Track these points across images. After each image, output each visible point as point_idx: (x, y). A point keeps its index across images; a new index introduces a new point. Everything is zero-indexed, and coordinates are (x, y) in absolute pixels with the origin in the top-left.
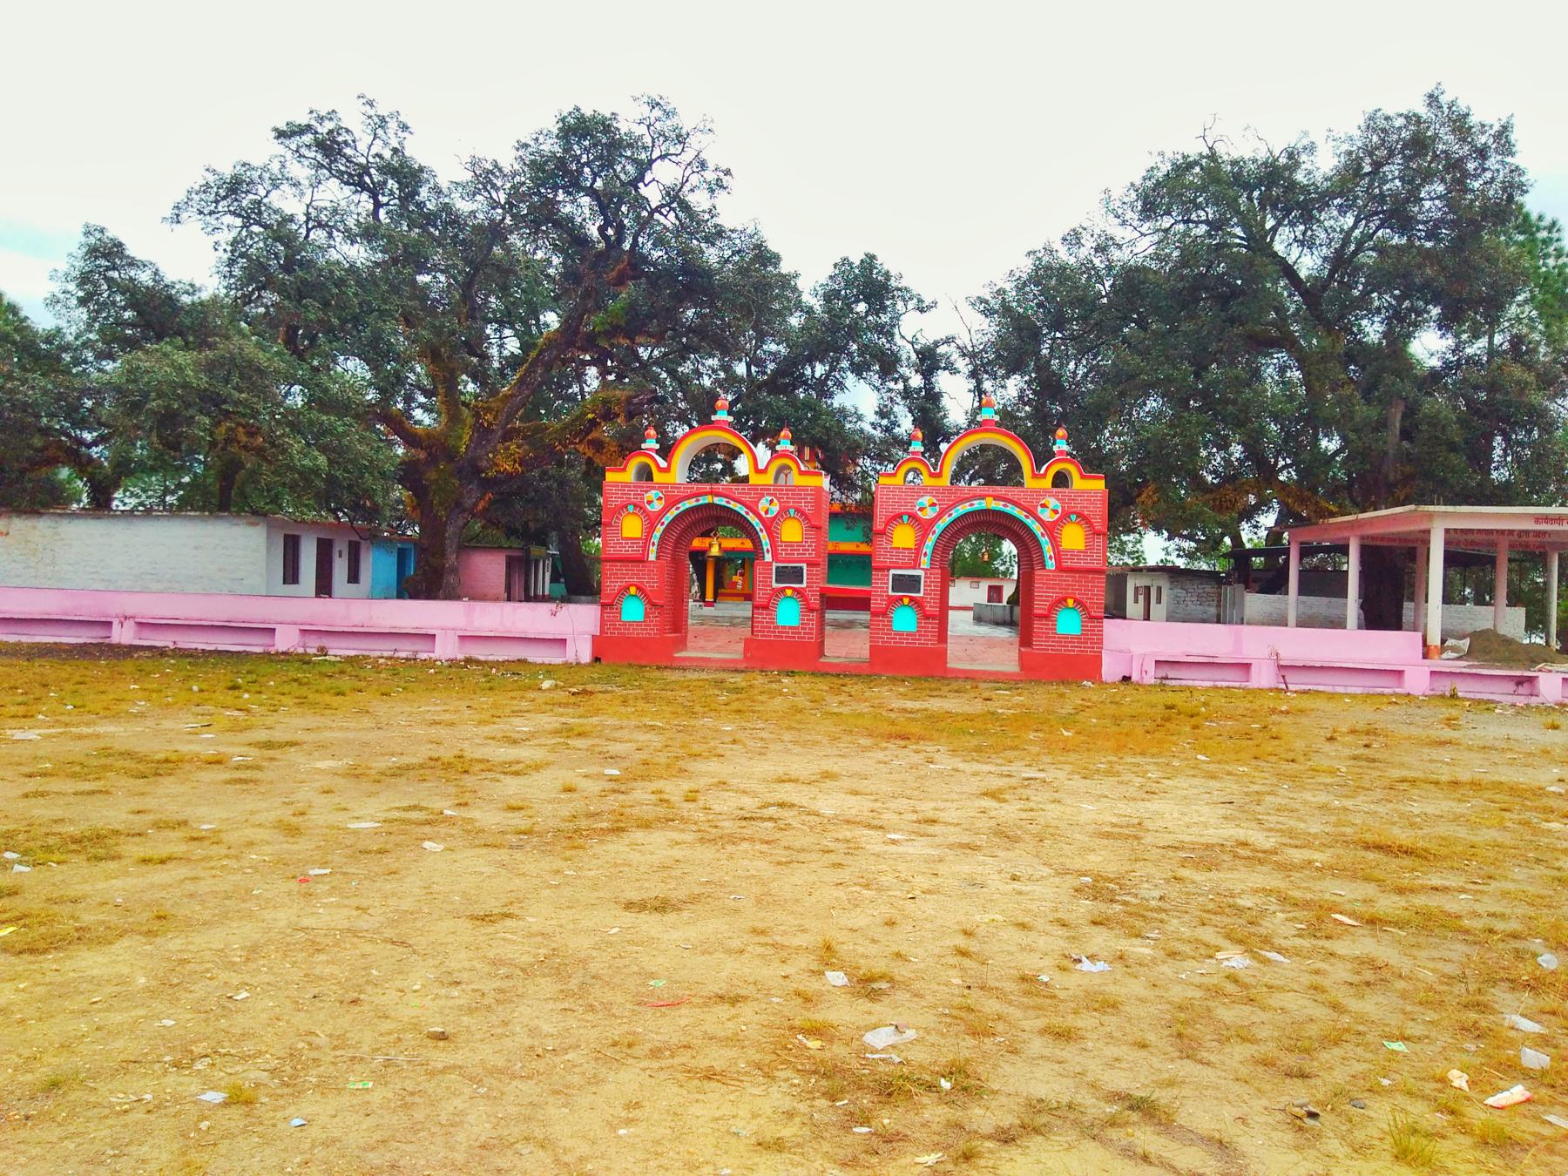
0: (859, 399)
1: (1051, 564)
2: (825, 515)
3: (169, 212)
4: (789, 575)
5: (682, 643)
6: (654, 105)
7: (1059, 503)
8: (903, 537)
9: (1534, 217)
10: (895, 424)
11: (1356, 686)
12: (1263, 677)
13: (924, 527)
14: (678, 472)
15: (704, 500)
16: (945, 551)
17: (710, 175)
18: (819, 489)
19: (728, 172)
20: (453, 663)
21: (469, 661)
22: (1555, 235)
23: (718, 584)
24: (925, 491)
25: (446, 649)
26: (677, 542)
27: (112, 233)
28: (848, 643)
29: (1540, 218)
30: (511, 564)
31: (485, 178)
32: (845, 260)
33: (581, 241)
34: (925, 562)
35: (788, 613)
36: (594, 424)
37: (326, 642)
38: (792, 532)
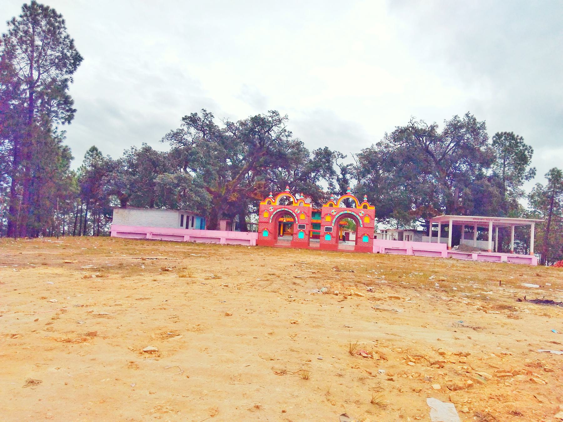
0: (323, 184)
1: (362, 226)
2: (311, 213)
3: (161, 140)
4: (302, 227)
5: (276, 242)
6: (273, 112)
7: (364, 212)
8: (328, 219)
9: (516, 136)
10: (334, 188)
11: (430, 255)
12: (409, 253)
13: (333, 217)
14: (277, 203)
15: (283, 209)
16: (338, 222)
17: (287, 134)
18: (309, 207)
19: (291, 132)
20: (224, 245)
21: (228, 244)
22: (522, 141)
23: (284, 231)
24: (334, 209)
25: (223, 242)
26: (276, 220)
27: (149, 145)
28: (315, 243)
29: (518, 136)
30: (227, 223)
31: (230, 126)
32: (320, 149)
33: (255, 145)
34: (333, 225)
35: (301, 235)
36: (256, 189)
37: (195, 239)
38: (302, 217)
